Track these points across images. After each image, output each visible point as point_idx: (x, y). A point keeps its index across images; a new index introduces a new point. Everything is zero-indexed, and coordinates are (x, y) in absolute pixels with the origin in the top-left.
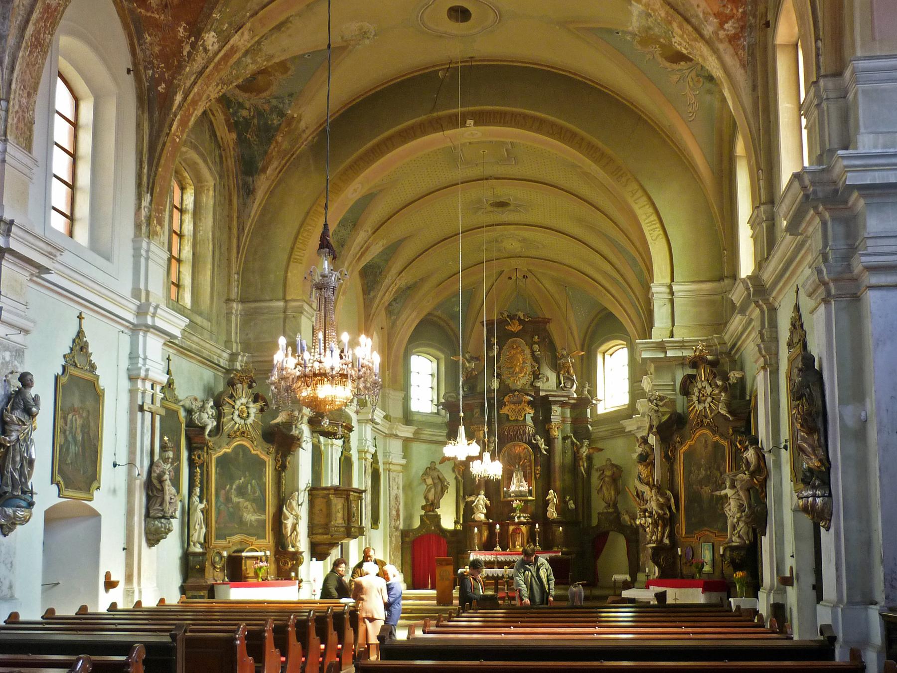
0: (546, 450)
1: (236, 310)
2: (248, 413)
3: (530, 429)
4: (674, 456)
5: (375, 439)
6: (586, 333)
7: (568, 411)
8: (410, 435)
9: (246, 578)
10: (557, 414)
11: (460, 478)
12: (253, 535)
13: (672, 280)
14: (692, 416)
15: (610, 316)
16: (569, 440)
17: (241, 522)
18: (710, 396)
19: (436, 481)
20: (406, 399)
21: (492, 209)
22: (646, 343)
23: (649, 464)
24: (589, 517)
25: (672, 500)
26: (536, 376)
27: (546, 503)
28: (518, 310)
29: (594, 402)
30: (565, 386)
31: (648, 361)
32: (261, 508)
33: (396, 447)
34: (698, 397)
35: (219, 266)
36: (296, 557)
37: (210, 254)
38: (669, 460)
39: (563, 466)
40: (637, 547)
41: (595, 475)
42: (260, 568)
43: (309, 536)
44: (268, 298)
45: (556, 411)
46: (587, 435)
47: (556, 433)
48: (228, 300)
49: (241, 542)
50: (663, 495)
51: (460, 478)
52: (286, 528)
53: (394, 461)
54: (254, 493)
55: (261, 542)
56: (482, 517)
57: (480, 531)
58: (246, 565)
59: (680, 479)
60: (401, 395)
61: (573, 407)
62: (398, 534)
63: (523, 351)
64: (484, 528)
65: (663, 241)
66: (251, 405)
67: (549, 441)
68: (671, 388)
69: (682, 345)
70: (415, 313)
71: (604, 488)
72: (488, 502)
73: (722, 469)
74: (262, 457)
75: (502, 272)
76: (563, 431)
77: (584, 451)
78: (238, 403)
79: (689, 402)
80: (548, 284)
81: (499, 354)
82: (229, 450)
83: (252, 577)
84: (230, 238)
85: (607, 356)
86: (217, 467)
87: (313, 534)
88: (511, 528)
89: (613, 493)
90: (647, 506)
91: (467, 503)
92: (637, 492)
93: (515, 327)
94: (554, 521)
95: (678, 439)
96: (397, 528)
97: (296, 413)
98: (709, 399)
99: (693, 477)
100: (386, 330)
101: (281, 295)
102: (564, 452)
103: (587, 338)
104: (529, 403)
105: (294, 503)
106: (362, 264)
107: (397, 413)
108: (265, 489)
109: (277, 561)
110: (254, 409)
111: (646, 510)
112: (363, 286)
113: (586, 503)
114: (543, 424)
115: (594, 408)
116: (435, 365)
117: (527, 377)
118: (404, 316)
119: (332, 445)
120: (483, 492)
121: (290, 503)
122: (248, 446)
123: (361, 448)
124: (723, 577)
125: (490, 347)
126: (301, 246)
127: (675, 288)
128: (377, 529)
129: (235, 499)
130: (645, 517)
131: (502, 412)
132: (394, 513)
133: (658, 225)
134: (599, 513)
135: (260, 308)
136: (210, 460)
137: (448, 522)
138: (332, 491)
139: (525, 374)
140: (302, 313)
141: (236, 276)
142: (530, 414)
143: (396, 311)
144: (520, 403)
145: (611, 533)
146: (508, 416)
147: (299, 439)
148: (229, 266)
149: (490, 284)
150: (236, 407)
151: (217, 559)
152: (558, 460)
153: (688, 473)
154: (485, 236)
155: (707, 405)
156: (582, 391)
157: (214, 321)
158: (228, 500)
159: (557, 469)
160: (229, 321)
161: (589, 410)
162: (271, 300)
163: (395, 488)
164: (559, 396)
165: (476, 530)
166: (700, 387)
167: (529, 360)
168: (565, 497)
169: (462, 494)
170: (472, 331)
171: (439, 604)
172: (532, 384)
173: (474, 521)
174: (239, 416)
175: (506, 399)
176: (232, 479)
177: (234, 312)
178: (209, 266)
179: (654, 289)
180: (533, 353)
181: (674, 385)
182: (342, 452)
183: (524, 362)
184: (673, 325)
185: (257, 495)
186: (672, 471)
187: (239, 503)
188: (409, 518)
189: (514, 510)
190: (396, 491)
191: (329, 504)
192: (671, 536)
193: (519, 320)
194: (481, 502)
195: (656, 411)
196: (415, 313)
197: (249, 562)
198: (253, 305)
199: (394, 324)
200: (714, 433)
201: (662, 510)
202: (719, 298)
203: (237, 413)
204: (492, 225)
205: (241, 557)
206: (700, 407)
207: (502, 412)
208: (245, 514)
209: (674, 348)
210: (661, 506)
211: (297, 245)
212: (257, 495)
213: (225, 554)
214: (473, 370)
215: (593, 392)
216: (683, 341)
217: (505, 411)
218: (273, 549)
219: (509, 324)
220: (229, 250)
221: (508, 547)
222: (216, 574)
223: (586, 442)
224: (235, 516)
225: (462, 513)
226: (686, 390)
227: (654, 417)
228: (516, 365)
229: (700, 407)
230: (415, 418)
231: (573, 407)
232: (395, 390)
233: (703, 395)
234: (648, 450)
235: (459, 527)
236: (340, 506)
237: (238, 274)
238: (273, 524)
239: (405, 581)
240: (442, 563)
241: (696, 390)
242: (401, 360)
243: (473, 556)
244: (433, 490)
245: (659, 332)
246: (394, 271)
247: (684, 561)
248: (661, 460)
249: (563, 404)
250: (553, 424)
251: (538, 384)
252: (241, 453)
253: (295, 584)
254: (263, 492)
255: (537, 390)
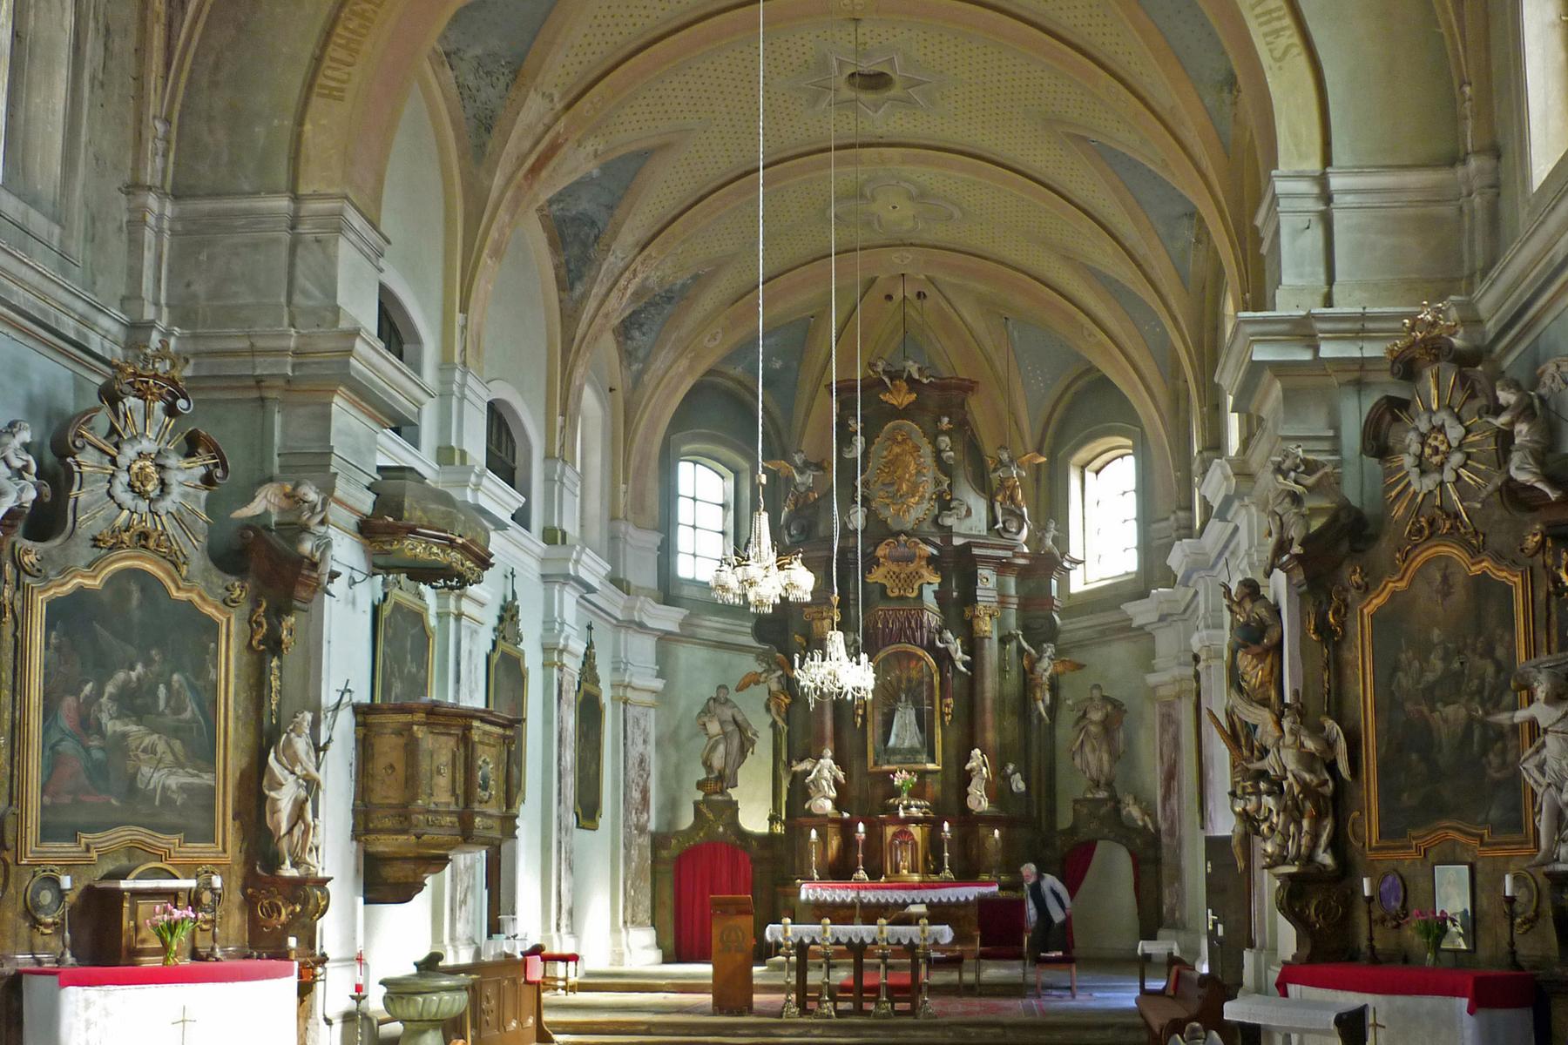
0: (965, 663)
1: (160, 217)
2: (163, 483)
3: (932, 618)
4: (1343, 625)
5: (590, 628)
6: (1047, 424)
7: (1011, 583)
8: (673, 627)
9: (135, 953)
10: (990, 585)
11: (781, 723)
12: (171, 830)
13: (1327, 160)
14: (1399, 511)
15: (1104, 383)
16: (1014, 644)
17: (131, 788)
18: (1460, 447)
19: (730, 728)
20: (667, 552)
21: (847, 93)
22: (1265, 321)
23: (1267, 651)
24: (1052, 811)
25: (1342, 745)
26: (945, 505)
27: (966, 778)
28: (906, 358)
29: (1066, 564)
30: (1005, 529)
31: (1267, 374)
32: (203, 752)
33: (642, 649)
34: (1420, 457)
35: (100, 85)
36: (307, 896)
37: (65, 39)
38: (1329, 639)
39: (1001, 700)
40: (1158, 873)
41: (1066, 718)
42: (172, 927)
43: (356, 835)
44: (246, 187)
45: (987, 579)
46: (1052, 634)
47: (986, 626)
48: (134, 188)
49: (131, 850)
50: (1317, 730)
51: (781, 723)
52: (275, 811)
53: (636, 682)
54: (178, 710)
55: (198, 850)
56: (828, 806)
57: (823, 836)
58: (134, 913)
59: (1363, 689)
60: (655, 539)
61: (1024, 574)
62: (645, 841)
63: (917, 448)
64: (832, 830)
65: (1301, 63)
66: (173, 461)
67: (973, 645)
68: (1326, 446)
69: (1359, 328)
70: (684, 363)
71: (1087, 749)
72: (841, 775)
73: (1500, 652)
74: (208, 610)
75: (873, 280)
76: (1001, 623)
77: (1046, 668)
78: (129, 452)
79: (1389, 473)
80: (970, 313)
81: (865, 454)
82: (94, 583)
83: (155, 952)
84: (143, 20)
85: (1089, 475)
86: (50, 626)
87: (367, 831)
88: (890, 831)
89: (1105, 757)
90: (1270, 763)
91: (795, 775)
92: (1232, 725)
93: (902, 398)
94: (981, 818)
95: (1356, 578)
96: (642, 829)
97: (312, 495)
98: (1457, 458)
99: (1405, 680)
100: (619, 394)
101: (282, 178)
102: (1002, 670)
103: (1050, 431)
104: (931, 560)
105: (301, 745)
106: (545, 191)
107: (644, 575)
108: (215, 703)
109: (249, 903)
110: (185, 474)
111: (1263, 774)
112: (556, 268)
113: (1045, 781)
114: (959, 605)
115: (1064, 583)
116: (730, 484)
117: (926, 505)
118: (659, 364)
119: (459, 616)
120: (828, 752)
121: (289, 742)
122: (161, 574)
123: (551, 641)
124: (1515, 964)
125: (845, 438)
126: (341, 54)
127: (1336, 182)
128: (595, 829)
129: (112, 726)
130: (1258, 793)
131: (871, 579)
132: (636, 795)
133: (1288, 21)
134: (1076, 801)
135: (231, 214)
136: (27, 606)
137: (755, 818)
138: (420, 717)
139: (922, 497)
140: (339, 230)
141: (160, 126)
142: (931, 584)
143: (641, 354)
144: (909, 559)
145: (1101, 845)
146: (883, 587)
147: (314, 566)
148: (140, 97)
149: (847, 308)
150: (123, 461)
151: (47, 897)
152: (990, 685)
153: (1387, 670)
154: (835, 176)
155: (1449, 476)
156: (1041, 540)
157: (79, 223)
158: (88, 724)
159: (989, 704)
160: (135, 245)
161: (1054, 582)
162: (255, 193)
163: (640, 741)
164: (993, 547)
165: (814, 833)
166: (1424, 426)
167: (930, 471)
168: (1003, 766)
169: (784, 757)
170: (807, 415)
171: (720, 1007)
172: (935, 521)
173: (809, 814)
174: (131, 486)
175: (881, 551)
176: (103, 668)
177: (151, 220)
178: (62, 75)
179: (1281, 186)
180: (938, 453)
181: (1336, 438)
182: (494, 643)
183: (919, 473)
184: (1331, 279)
185: (187, 715)
186: (1337, 666)
187: (125, 735)
188: (671, 806)
189: (896, 792)
190: (640, 748)
191: (411, 749)
192: (1338, 845)
193: (911, 381)
194: (826, 774)
195: (1296, 499)
196: (684, 363)
197: (143, 906)
198: (207, 205)
199: (637, 379)
200: (1475, 553)
201: (1311, 771)
202: (1448, 210)
203: (123, 478)
204: (852, 146)
205: (120, 892)
206: (1429, 483)
207: (871, 579)
208: (146, 770)
209: (1339, 336)
210: (1307, 760)
211: (332, 51)
212: (187, 715)
213: (66, 882)
214: (809, 489)
215: (1063, 540)
216: (1363, 317)
217: (877, 576)
218: (238, 870)
219: (886, 389)
220: (141, 51)
221: (881, 872)
222: (39, 940)
223: (1050, 649)
224: (113, 774)
225: (784, 798)
226: (1378, 444)
227: (1290, 518)
228: (901, 478)
229: (1422, 485)
230: (686, 592)
231: (1024, 574)
232: (638, 527)
233: (1436, 451)
234: (1263, 613)
235: (779, 829)
236: (444, 758)
237: (167, 121)
238: (239, 801)
239: (659, 945)
240: (727, 909)
241: (1412, 439)
242: (654, 464)
243: (807, 892)
244: (721, 748)
245: (1295, 291)
246: (628, 236)
247: (1377, 914)
248: (1304, 636)
249: (1002, 567)
250: (980, 606)
251: (948, 521)
252: (136, 596)
253: (288, 974)
254: (209, 708)
255: (948, 532)
